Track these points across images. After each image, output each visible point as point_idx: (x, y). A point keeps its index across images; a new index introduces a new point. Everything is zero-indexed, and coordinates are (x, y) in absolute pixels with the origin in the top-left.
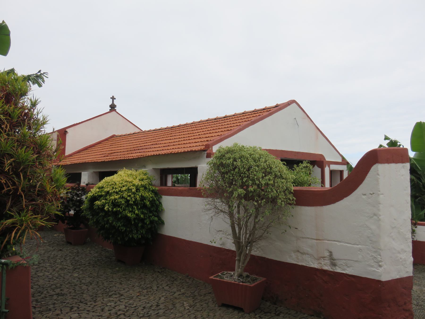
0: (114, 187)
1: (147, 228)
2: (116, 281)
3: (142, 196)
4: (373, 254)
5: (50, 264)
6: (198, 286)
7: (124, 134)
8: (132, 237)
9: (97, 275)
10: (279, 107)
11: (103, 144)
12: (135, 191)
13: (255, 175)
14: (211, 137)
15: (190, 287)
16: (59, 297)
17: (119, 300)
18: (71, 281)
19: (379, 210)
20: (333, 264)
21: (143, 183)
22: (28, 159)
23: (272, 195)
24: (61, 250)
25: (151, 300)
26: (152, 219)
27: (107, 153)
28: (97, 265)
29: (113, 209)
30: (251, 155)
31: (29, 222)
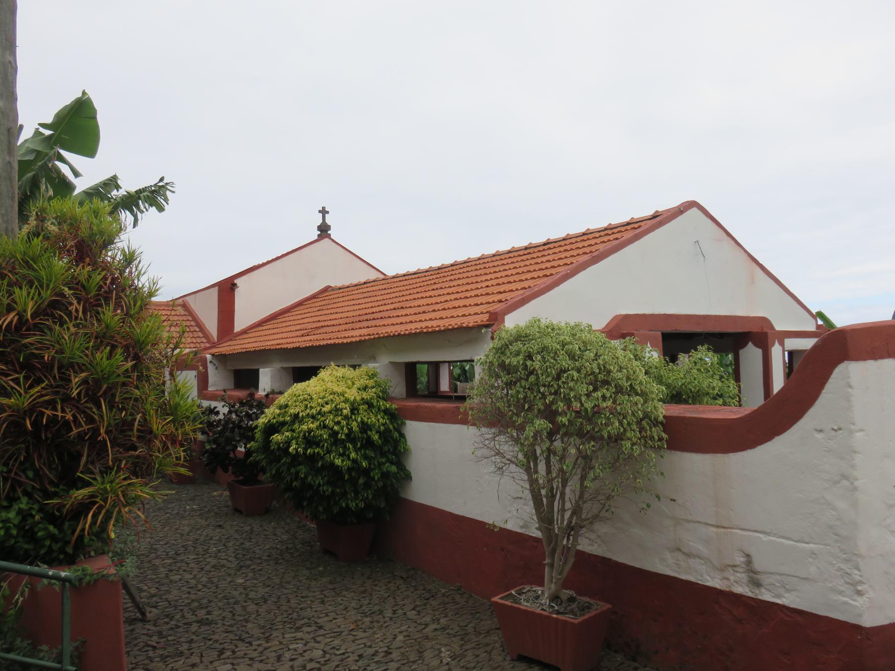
0: (309, 406)
1: (376, 488)
2: (314, 597)
3: (362, 422)
4: (843, 566)
5: (196, 556)
6: (476, 613)
7: (347, 283)
8: (347, 506)
9: (281, 582)
10: (658, 219)
11: (306, 306)
12: (349, 414)
13: (571, 389)
14: (539, 270)
15: (461, 613)
16: (202, 627)
17: (314, 638)
18: (229, 593)
19: (853, 467)
20: (754, 583)
21: (365, 395)
22: (114, 371)
23: (609, 432)
24: (220, 526)
25: (377, 640)
26: (385, 469)
27: (310, 327)
28: (283, 559)
29: (305, 449)
30: (566, 344)
31: (120, 493)
